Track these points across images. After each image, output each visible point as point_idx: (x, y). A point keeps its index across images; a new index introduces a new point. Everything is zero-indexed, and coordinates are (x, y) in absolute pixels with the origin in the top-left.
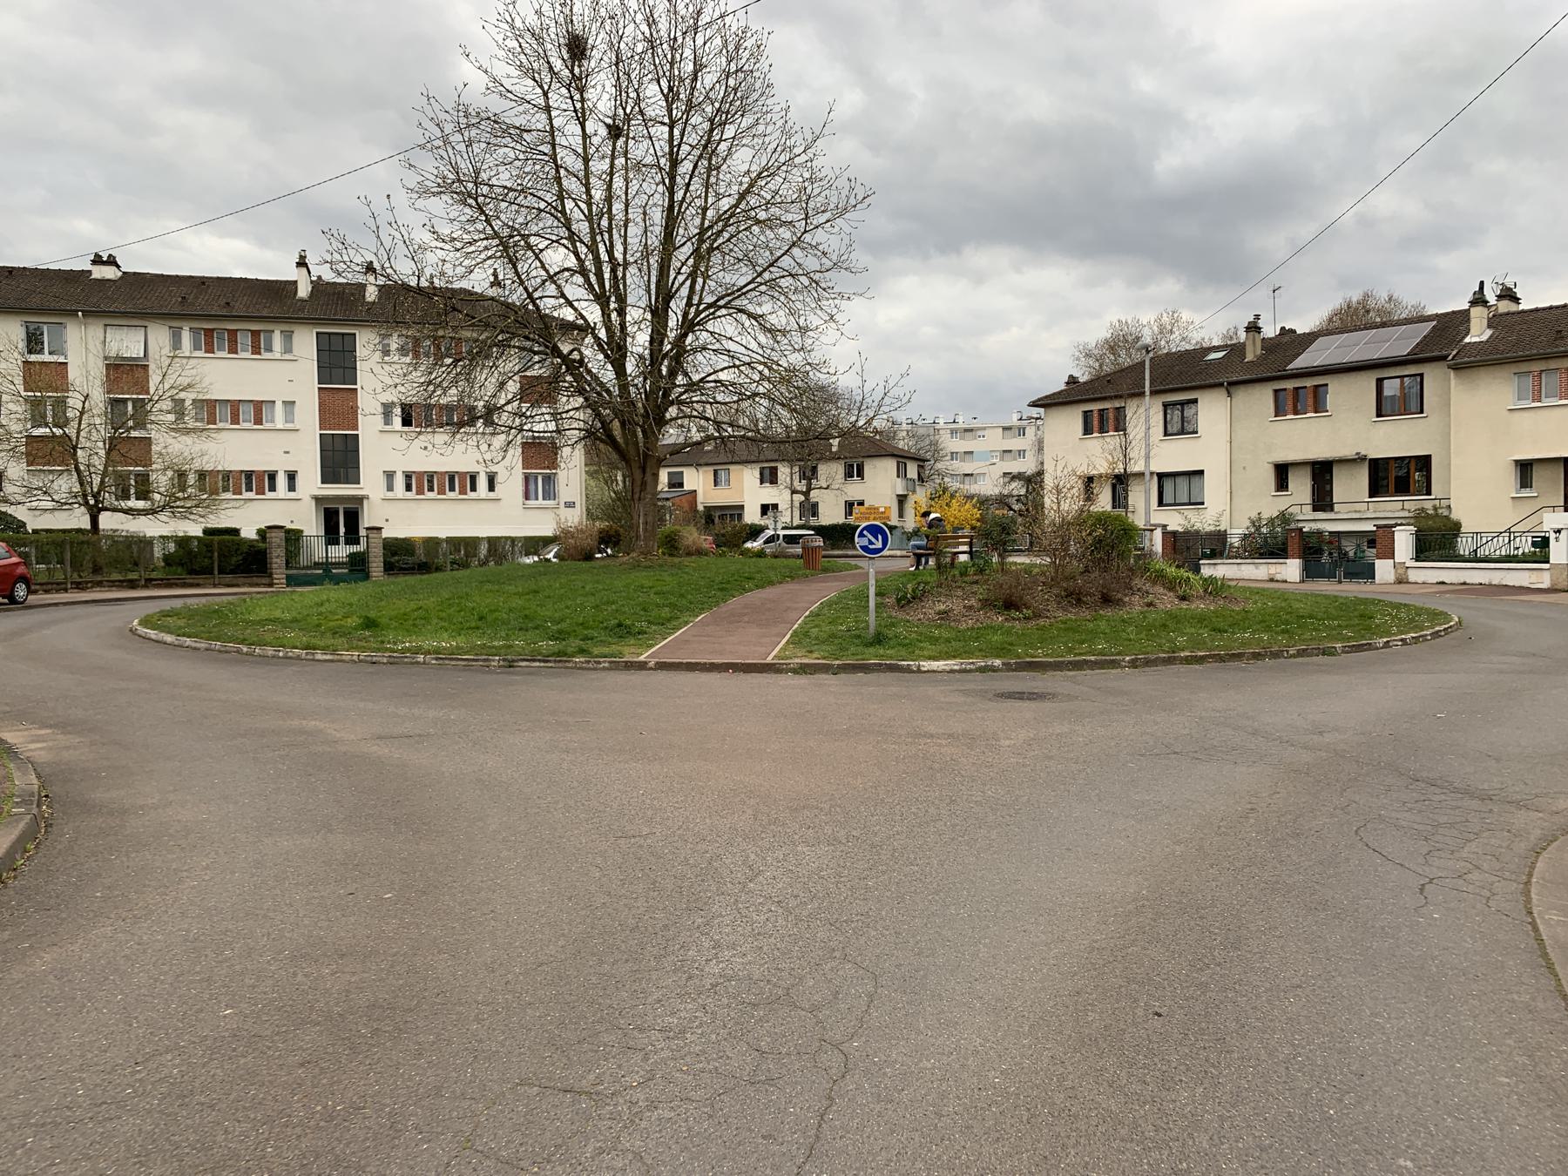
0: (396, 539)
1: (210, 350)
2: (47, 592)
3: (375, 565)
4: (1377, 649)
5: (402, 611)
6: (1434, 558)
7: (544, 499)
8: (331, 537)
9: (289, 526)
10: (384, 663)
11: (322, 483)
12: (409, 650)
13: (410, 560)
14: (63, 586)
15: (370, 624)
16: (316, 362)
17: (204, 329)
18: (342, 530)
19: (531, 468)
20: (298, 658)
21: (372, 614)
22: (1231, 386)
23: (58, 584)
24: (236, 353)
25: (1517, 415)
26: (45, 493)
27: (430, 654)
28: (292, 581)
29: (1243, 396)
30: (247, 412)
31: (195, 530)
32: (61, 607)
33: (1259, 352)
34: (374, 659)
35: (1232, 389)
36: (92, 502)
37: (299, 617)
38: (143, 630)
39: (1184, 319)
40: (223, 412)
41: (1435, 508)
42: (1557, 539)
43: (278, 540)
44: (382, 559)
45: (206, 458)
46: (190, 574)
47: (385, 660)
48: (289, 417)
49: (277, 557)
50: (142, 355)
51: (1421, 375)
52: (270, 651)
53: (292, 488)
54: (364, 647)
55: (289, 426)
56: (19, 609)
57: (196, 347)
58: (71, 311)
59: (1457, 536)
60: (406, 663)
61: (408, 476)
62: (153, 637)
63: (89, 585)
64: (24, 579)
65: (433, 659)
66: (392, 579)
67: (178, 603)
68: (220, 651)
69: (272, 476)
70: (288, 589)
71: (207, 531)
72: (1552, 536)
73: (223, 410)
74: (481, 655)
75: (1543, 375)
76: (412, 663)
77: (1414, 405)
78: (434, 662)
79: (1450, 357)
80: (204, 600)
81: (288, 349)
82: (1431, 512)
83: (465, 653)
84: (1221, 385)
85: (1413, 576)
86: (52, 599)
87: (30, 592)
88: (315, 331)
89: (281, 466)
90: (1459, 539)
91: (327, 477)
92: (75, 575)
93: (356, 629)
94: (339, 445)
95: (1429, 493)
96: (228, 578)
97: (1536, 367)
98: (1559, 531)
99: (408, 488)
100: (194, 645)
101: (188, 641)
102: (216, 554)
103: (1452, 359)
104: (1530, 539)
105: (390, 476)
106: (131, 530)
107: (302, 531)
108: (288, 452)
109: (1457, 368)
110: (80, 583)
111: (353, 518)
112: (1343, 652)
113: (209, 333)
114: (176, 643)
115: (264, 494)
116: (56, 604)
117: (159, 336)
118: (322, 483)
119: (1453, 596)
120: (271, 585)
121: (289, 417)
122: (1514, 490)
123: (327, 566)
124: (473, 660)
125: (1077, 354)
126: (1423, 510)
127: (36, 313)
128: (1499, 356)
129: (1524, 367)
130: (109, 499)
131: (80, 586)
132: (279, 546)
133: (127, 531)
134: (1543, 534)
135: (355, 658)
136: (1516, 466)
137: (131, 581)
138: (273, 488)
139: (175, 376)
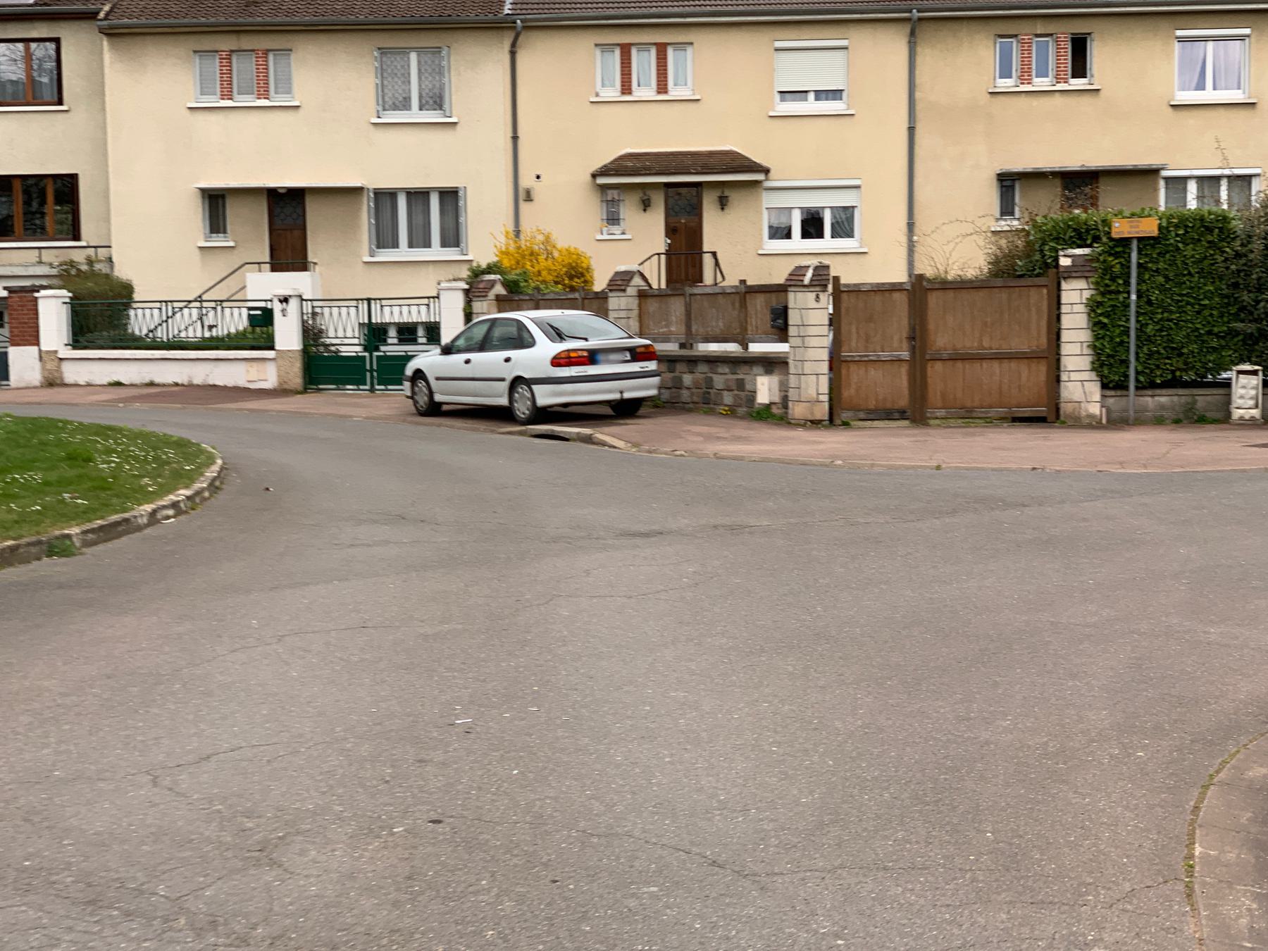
4: (140, 528)
6: (100, 342)
7: (411, 245)
25: (200, 116)
41: (90, 262)
42: (284, 312)
51: (57, 41)
59: (127, 306)
72: (277, 307)
75: (271, 57)
77: (48, 94)
79: (102, 15)
82: (84, 268)
85: (72, 373)
90: (132, 313)
95: (77, 237)
97: (226, 43)
98: (285, 300)
103: (106, 19)
104: (245, 312)
109: (113, 33)
112: (87, 544)
119: (146, 406)
122: (202, 236)
126: (72, 264)
128: (172, 21)
129: (208, 43)
134: (262, 304)
136: (203, 197)
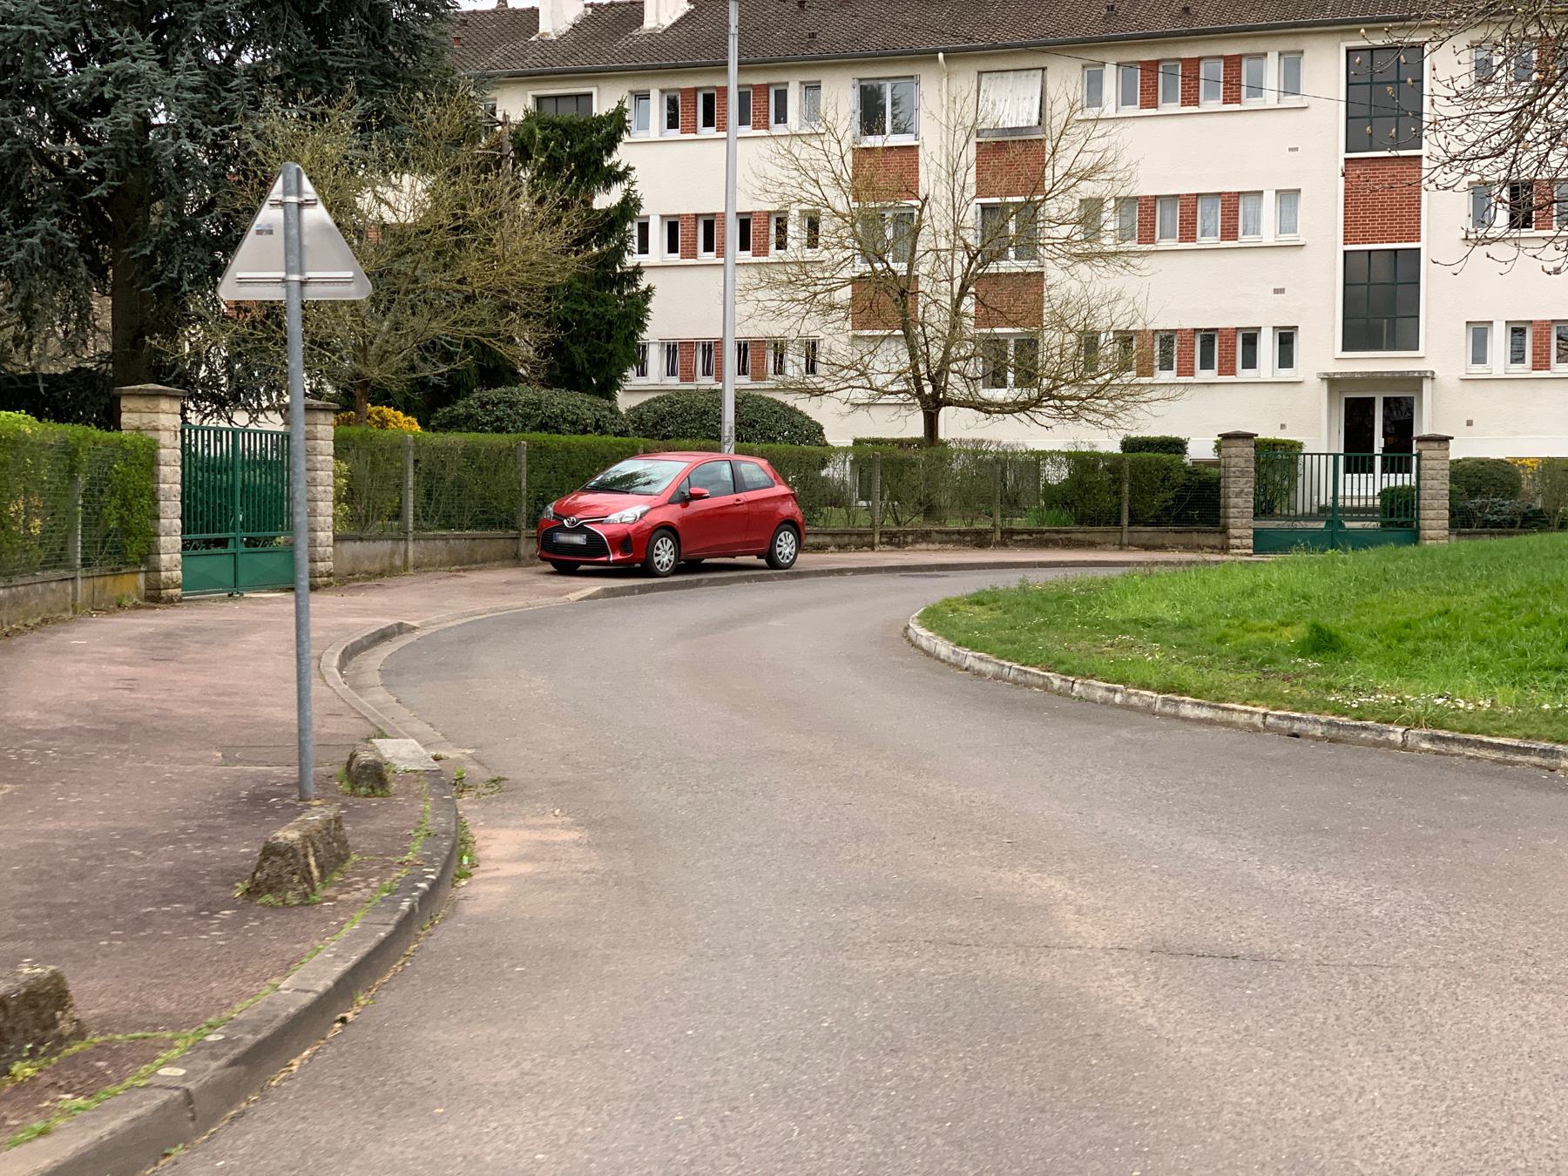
0: (1482, 462)
1: (1150, 101)
2: (842, 548)
3: (1431, 514)
5: (1401, 619)
8: (1356, 456)
9: (1266, 432)
10: (1316, 739)
12: (1373, 712)
13: (1508, 505)
14: (867, 539)
15: (1322, 643)
16: (1343, 105)
17: (1140, 62)
18: (1379, 443)
20: (1148, 710)
21: (1330, 622)
23: (860, 535)
24: (1197, 103)
26: (862, 374)
27: (1418, 725)
28: (1263, 543)
30: (1210, 218)
31: (1108, 443)
32: (849, 577)
34: (1297, 727)
36: (928, 390)
37: (1197, 618)
38: (923, 635)
40: (1168, 222)
43: (1241, 462)
45: (1119, 307)
46: (1080, 522)
47: (1319, 731)
48: (1287, 222)
49: (1238, 495)
50: (1035, 118)
52: (1099, 689)
53: (1286, 359)
54: (1282, 697)
55: (1287, 238)
56: (781, 577)
57: (1127, 100)
58: (925, 52)
60: (1364, 742)
61: (1517, 331)
62: (924, 643)
63: (910, 539)
64: (791, 524)
65: (1425, 737)
66: (1464, 543)
67: (1011, 580)
68: (1016, 683)
69: (1251, 339)
70: (1255, 558)
71: (1130, 445)
73: (1168, 214)
74: (1539, 738)
76: (1376, 744)
78: (1426, 745)
80: (1059, 574)
81: (1291, 86)
83: (1501, 732)
86: (850, 561)
87: (800, 547)
88: (530, 94)
89: (1266, 317)
91: (1357, 335)
92: (889, 521)
93: (1289, 653)
94: (1381, 272)
96: (1146, 533)
99: (1517, 356)
100: (978, 666)
101: (970, 658)
102: (1126, 487)
105: (1479, 332)
106: (1005, 441)
107: (1300, 445)
108: (1281, 291)
110: (894, 535)
113: (1150, 68)
114: (953, 659)
115: (1233, 373)
116: (841, 572)
117: (1065, 79)
120: (1225, 549)
121: (1287, 222)
123: (1333, 514)
124: (1518, 750)
127: (753, 70)
130: (956, 385)
131: (895, 540)
132: (1243, 473)
133: (998, 444)
135: (1257, 720)
137: (978, 533)
138: (1250, 362)
139: (1072, 153)
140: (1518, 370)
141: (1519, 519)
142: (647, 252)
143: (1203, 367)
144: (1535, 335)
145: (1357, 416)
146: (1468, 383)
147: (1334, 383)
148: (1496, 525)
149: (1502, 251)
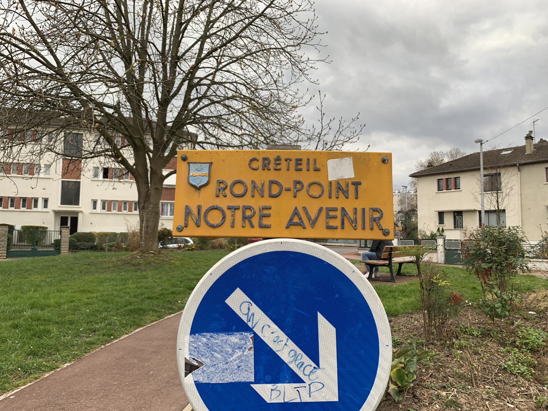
11: (61, 204)
19: (165, 200)
22: (521, 166)
29: (526, 170)
33: (533, 150)
35: (521, 168)
39: (462, 152)
44: (68, 244)
53: (46, 206)
55: (47, 176)
61: (104, 202)
69: (36, 200)
84: (515, 165)
89: (39, 194)
99: (104, 208)
105: (95, 203)
107: (47, 228)
111: (75, 221)
118: (61, 204)
125: (417, 165)
138: (36, 206)
140: (104, 211)
141: (89, 248)
142: (302, 159)
143: (23, 207)
144: (129, 204)
145: (64, 221)
146: (91, 214)
147: (56, 213)
148: (83, 249)
149: (99, 183)
